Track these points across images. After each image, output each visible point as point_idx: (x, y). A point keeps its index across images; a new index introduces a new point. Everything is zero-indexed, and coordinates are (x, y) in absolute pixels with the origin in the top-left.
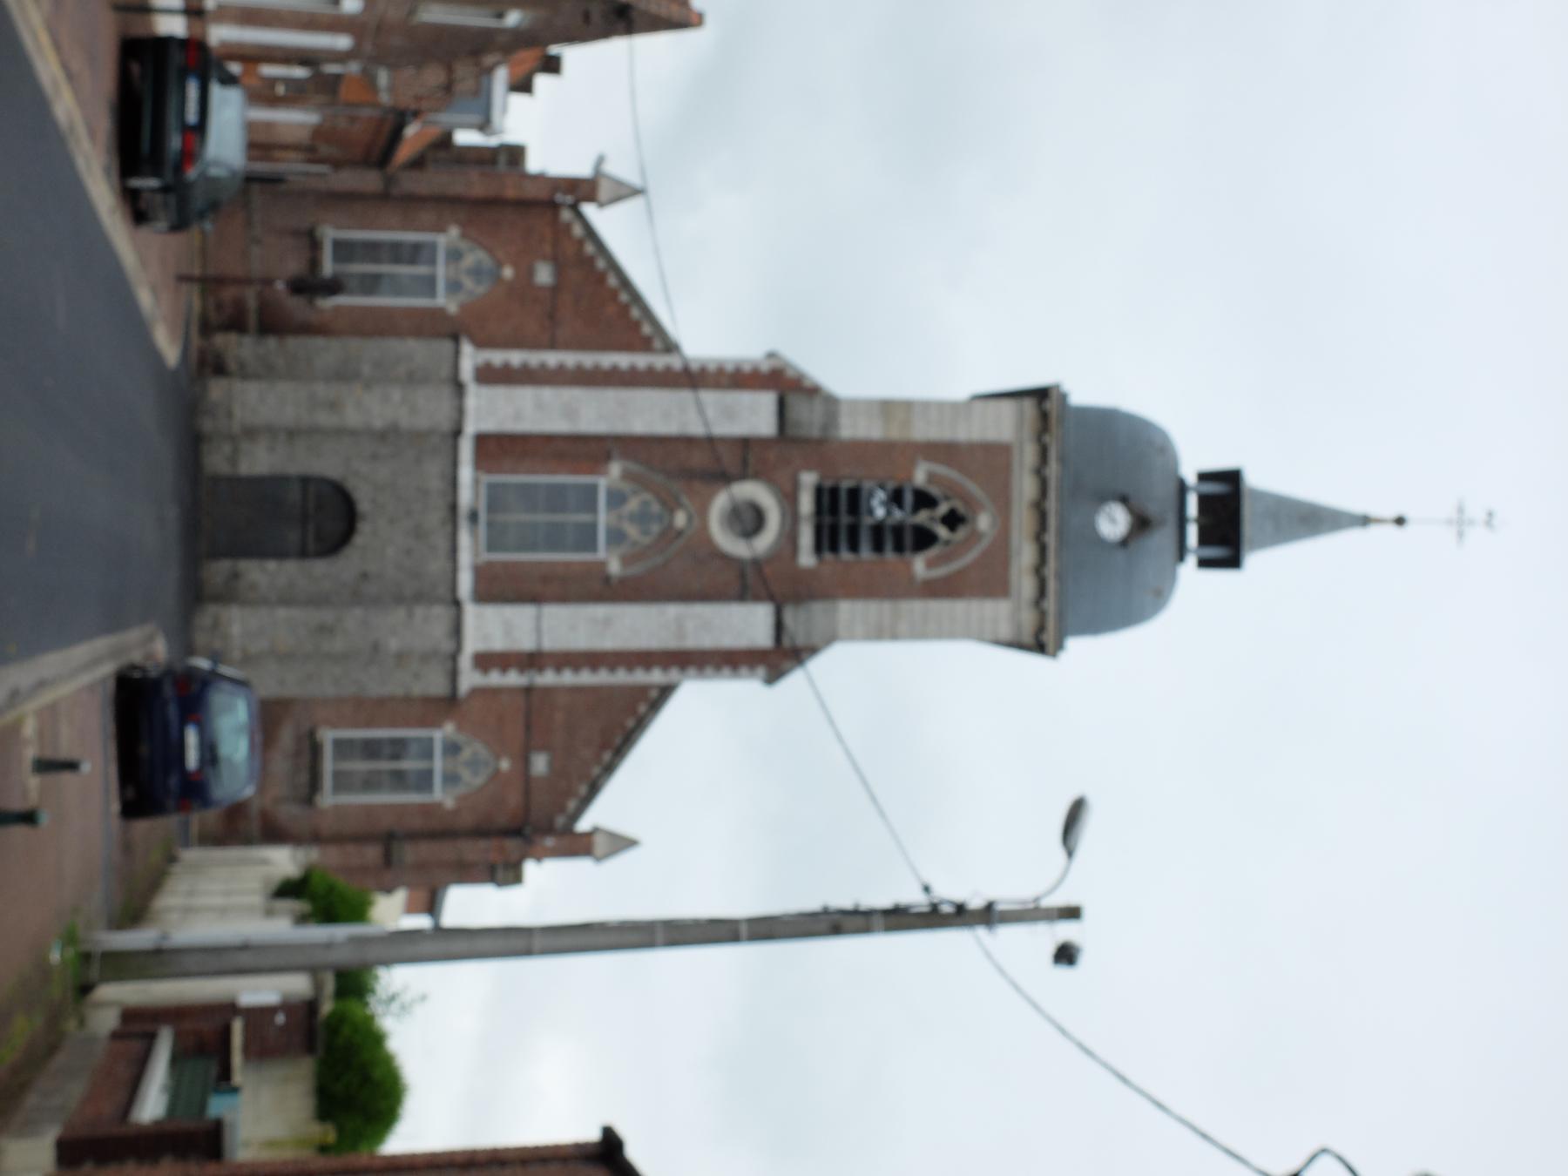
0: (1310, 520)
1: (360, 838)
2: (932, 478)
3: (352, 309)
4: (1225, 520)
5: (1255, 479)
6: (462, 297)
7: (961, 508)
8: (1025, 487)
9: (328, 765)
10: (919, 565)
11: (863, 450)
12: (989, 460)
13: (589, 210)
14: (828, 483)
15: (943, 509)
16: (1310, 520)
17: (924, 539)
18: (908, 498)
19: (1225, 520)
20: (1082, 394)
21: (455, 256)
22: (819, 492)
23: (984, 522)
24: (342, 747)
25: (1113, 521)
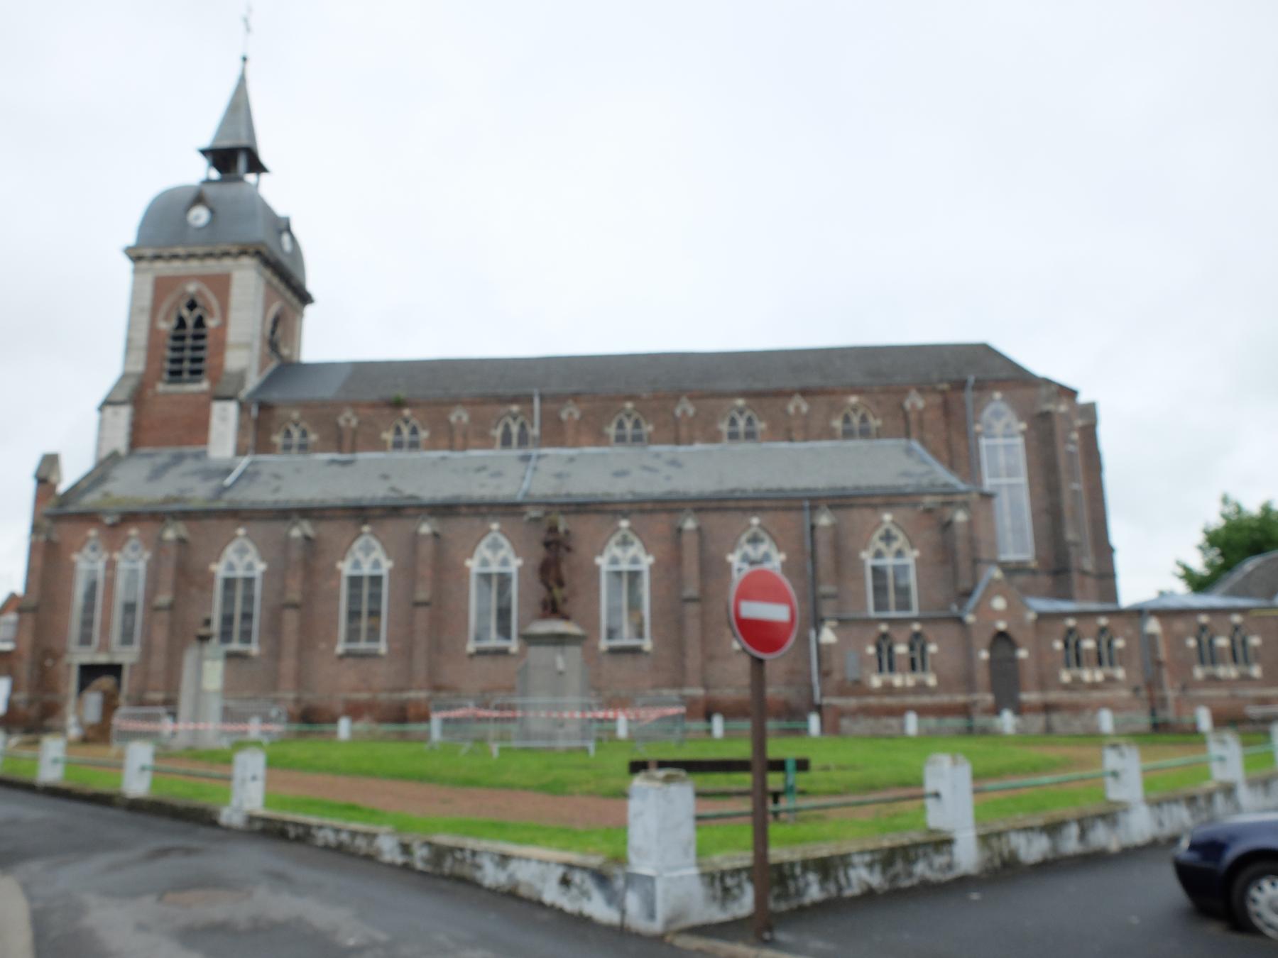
0: (239, 107)
1: (680, 624)
2: (167, 318)
3: (520, 595)
4: (233, 157)
5: (206, 141)
6: (907, 550)
7: (185, 301)
8: (176, 267)
9: (362, 646)
10: (211, 323)
11: (150, 359)
12: (162, 287)
13: (62, 487)
14: (166, 376)
15: (185, 313)
16: (239, 107)
17: (200, 323)
18: (181, 332)
19: (233, 157)
20: (131, 239)
21: (879, 554)
22: (170, 382)
23: (192, 288)
24: (353, 636)
25: (197, 217)
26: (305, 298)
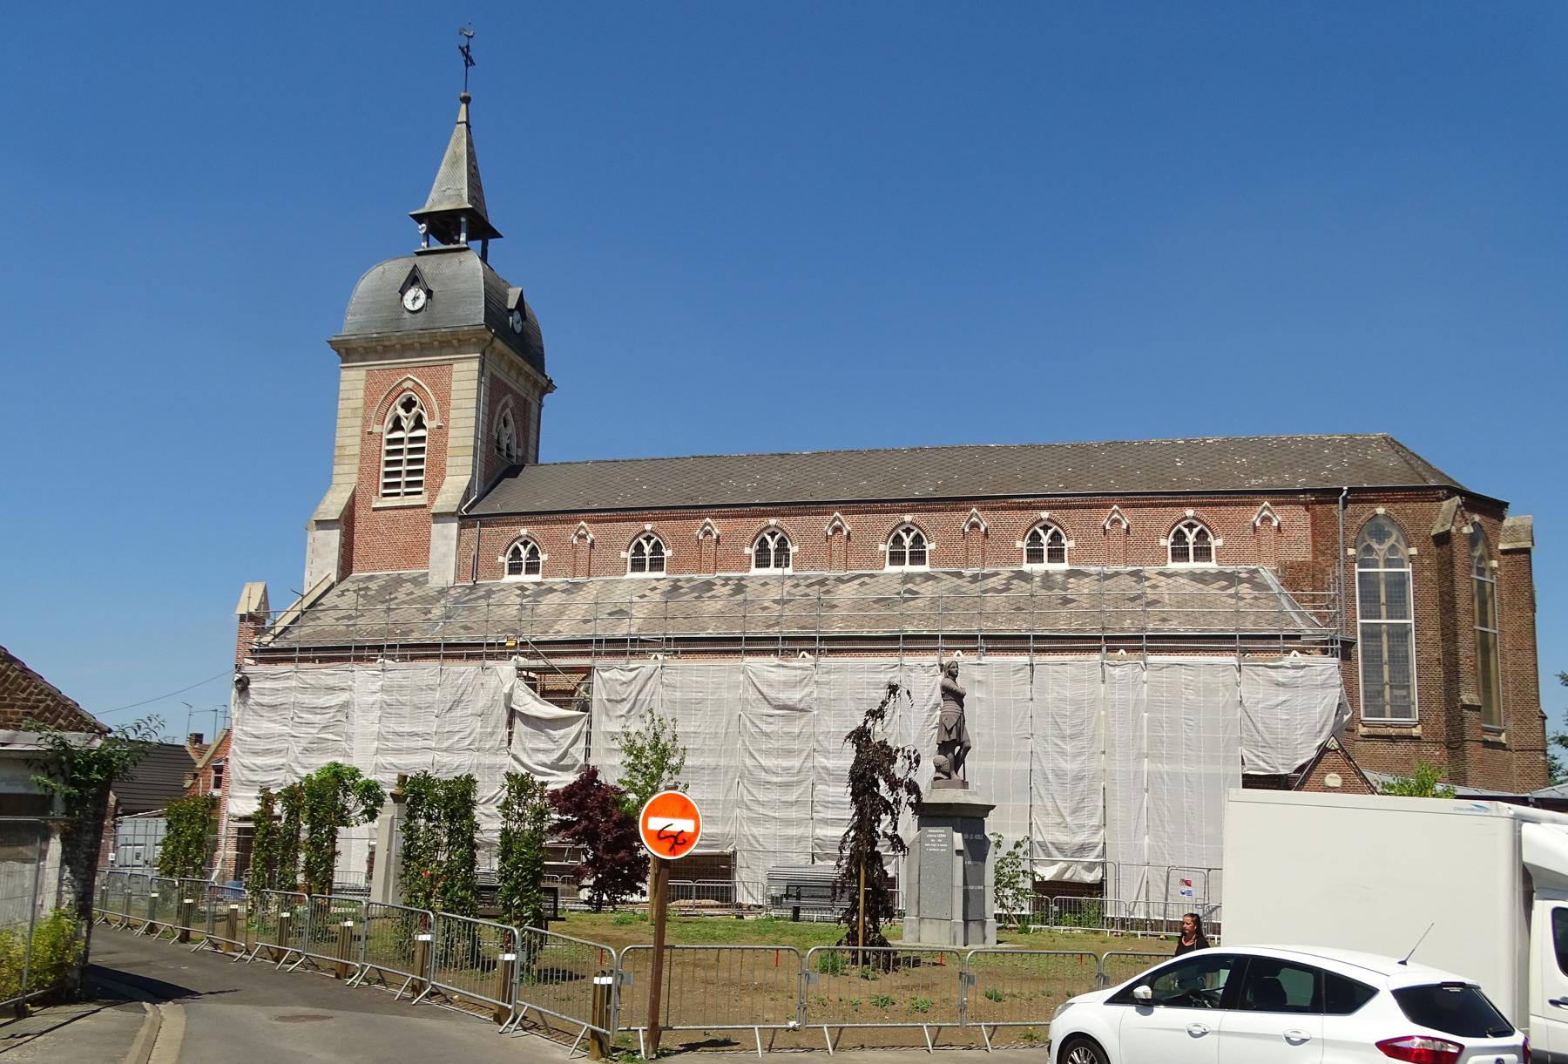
26: (549, 387)
